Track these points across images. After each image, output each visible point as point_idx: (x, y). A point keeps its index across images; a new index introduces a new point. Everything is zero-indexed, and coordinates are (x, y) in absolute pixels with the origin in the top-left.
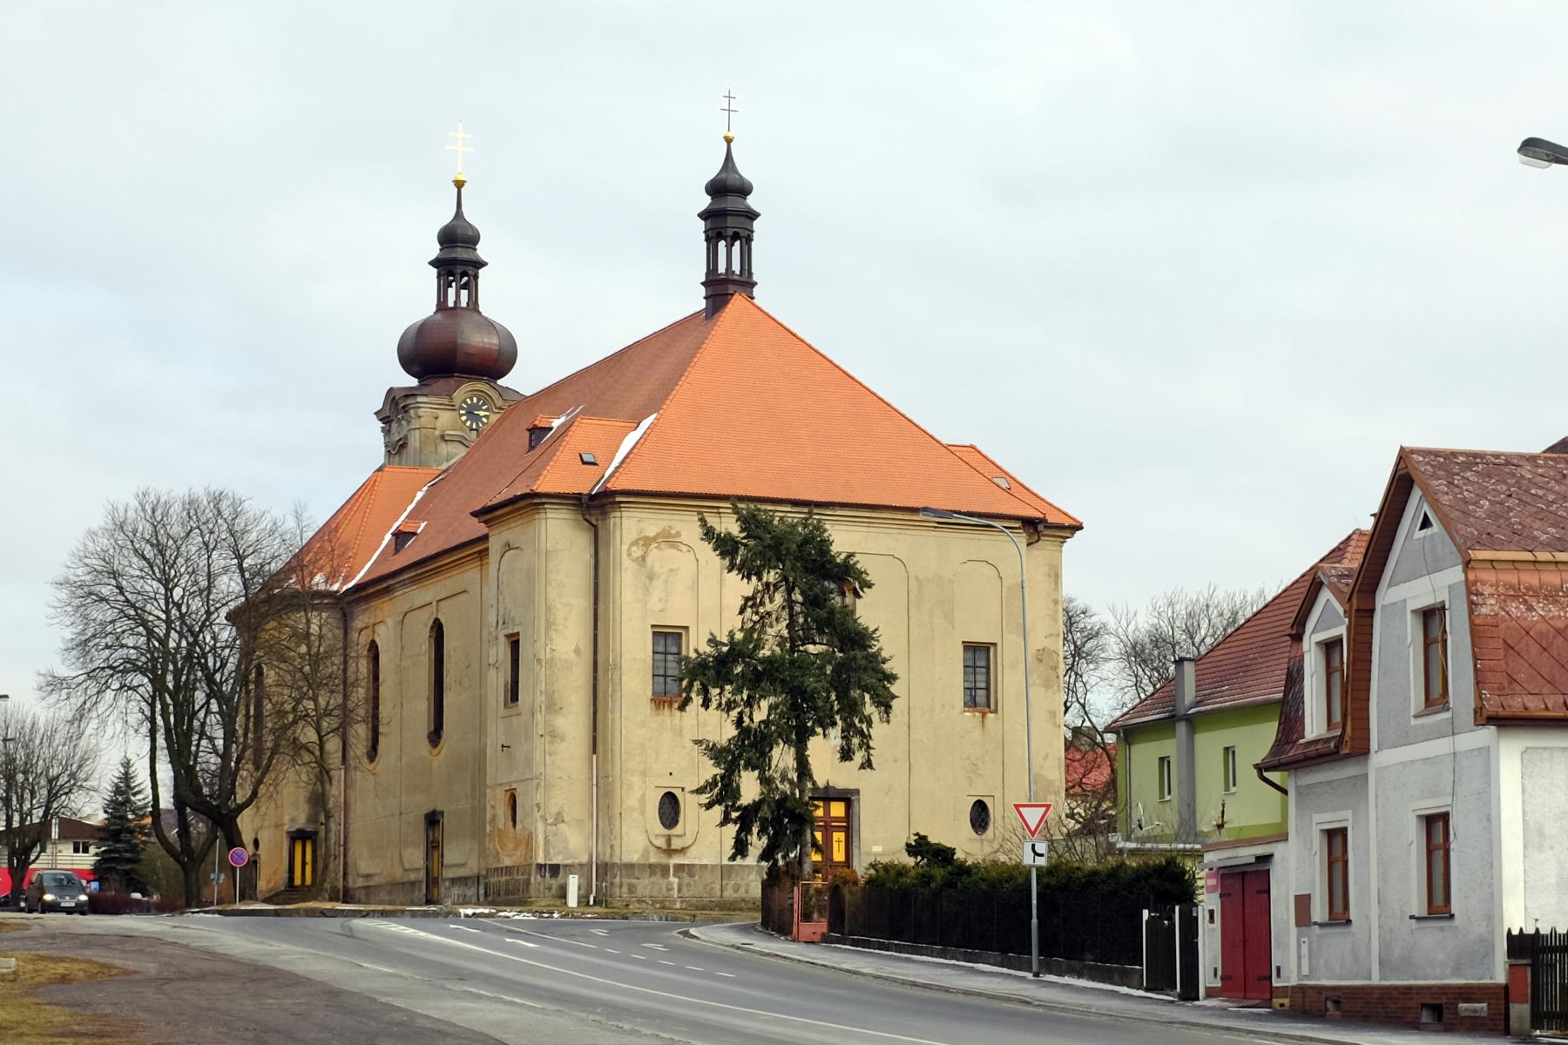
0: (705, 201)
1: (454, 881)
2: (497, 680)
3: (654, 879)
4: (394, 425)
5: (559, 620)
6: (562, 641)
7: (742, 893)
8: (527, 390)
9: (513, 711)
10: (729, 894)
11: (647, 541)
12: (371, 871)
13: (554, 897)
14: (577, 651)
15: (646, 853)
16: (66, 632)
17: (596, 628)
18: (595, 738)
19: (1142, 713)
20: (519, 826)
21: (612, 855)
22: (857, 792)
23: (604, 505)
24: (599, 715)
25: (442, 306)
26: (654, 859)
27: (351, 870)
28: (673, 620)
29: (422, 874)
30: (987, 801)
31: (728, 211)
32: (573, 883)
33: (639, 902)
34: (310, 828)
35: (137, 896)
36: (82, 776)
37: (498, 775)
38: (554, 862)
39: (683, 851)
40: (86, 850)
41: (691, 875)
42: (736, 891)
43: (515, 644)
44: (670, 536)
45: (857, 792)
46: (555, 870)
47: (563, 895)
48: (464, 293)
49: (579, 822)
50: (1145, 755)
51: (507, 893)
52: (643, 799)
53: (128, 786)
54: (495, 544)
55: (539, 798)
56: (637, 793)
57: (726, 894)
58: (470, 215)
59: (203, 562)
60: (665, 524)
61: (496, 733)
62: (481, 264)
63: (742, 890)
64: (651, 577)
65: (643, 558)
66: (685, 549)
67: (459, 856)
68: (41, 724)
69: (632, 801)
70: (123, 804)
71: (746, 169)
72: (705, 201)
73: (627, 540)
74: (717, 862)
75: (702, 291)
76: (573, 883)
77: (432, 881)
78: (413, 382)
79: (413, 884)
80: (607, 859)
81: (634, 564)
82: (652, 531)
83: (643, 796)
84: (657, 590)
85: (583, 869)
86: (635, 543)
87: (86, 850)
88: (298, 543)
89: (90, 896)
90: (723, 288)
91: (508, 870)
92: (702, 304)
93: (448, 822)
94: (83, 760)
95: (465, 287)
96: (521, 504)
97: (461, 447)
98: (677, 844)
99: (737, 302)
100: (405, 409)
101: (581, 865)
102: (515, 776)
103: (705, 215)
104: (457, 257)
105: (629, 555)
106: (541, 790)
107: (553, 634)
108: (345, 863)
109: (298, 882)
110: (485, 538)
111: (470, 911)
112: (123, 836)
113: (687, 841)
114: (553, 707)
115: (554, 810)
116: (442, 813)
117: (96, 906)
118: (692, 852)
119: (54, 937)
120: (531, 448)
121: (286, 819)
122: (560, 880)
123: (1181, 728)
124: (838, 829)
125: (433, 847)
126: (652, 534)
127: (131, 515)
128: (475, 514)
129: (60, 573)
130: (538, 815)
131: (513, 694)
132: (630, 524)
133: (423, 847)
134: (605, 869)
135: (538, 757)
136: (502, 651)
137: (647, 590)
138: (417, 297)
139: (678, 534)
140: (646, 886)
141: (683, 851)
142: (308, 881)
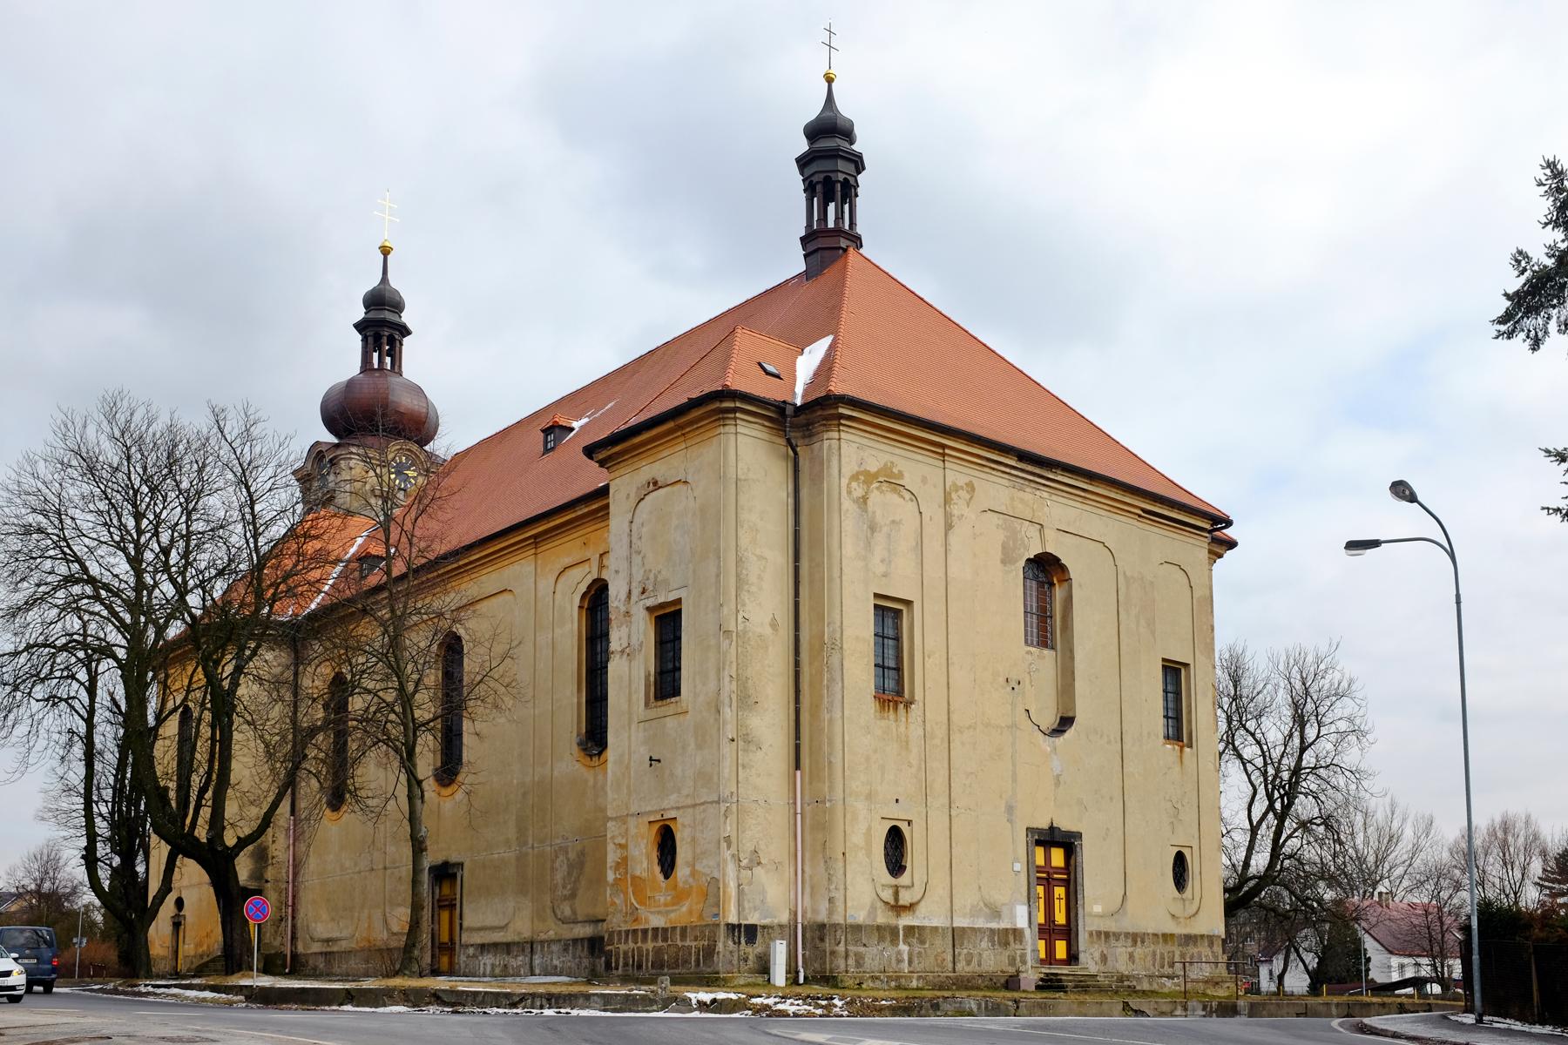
1: (483, 948)
5: (753, 579)
6: (749, 612)
11: (868, 478)
12: (335, 935)
13: (751, 971)
14: (774, 625)
15: (873, 908)
17: (797, 594)
20: (682, 871)
21: (831, 912)
22: (1079, 835)
26: (883, 918)
31: (830, 159)
39: (911, 907)
41: (922, 942)
44: (892, 475)
45: (1079, 835)
46: (751, 932)
47: (764, 968)
49: (777, 865)
54: (619, 503)
55: (729, 829)
56: (863, 827)
57: (959, 967)
58: (394, 282)
60: (887, 458)
62: (405, 331)
63: (975, 960)
64: (873, 528)
65: (865, 499)
66: (908, 496)
69: (857, 838)
71: (846, 108)
72: (803, 146)
73: (849, 468)
74: (948, 924)
80: (822, 917)
81: (855, 507)
82: (873, 466)
83: (869, 829)
84: (880, 538)
85: (788, 931)
86: (855, 477)
89: (1338, 902)
90: (828, 245)
98: (905, 898)
100: (333, 462)
101: (781, 926)
102: (672, 800)
104: (382, 326)
105: (849, 493)
106: (732, 818)
107: (745, 596)
108: (294, 926)
110: (603, 492)
111: (706, 997)
114: (746, 701)
115: (749, 847)
118: (922, 909)
120: (547, 451)
122: (758, 948)
126: (873, 469)
128: (590, 451)
130: (728, 854)
131: (666, 683)
132: (851, 452)
134: (819, 932)
135: (727, 769)
137: (868, 545)
139: (901, 474)
140: (875, 956)
141: (911, 907)
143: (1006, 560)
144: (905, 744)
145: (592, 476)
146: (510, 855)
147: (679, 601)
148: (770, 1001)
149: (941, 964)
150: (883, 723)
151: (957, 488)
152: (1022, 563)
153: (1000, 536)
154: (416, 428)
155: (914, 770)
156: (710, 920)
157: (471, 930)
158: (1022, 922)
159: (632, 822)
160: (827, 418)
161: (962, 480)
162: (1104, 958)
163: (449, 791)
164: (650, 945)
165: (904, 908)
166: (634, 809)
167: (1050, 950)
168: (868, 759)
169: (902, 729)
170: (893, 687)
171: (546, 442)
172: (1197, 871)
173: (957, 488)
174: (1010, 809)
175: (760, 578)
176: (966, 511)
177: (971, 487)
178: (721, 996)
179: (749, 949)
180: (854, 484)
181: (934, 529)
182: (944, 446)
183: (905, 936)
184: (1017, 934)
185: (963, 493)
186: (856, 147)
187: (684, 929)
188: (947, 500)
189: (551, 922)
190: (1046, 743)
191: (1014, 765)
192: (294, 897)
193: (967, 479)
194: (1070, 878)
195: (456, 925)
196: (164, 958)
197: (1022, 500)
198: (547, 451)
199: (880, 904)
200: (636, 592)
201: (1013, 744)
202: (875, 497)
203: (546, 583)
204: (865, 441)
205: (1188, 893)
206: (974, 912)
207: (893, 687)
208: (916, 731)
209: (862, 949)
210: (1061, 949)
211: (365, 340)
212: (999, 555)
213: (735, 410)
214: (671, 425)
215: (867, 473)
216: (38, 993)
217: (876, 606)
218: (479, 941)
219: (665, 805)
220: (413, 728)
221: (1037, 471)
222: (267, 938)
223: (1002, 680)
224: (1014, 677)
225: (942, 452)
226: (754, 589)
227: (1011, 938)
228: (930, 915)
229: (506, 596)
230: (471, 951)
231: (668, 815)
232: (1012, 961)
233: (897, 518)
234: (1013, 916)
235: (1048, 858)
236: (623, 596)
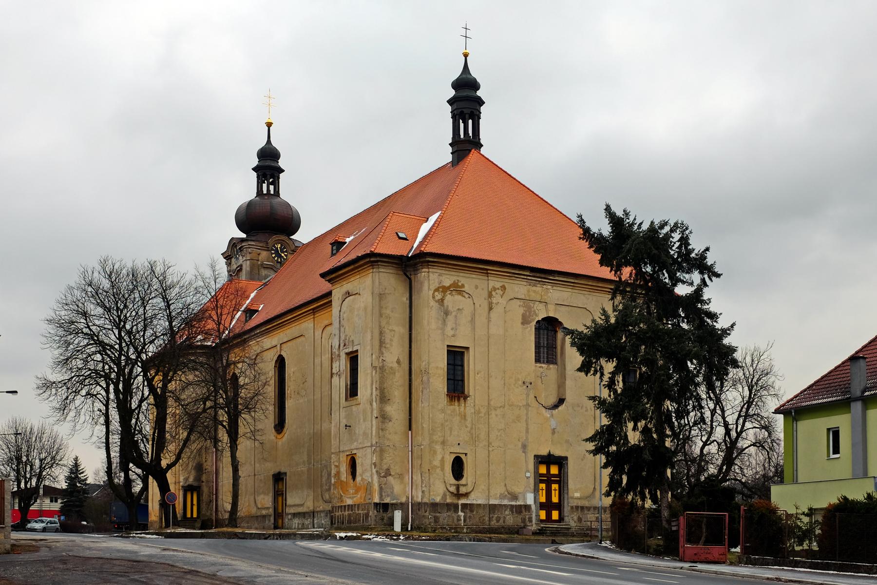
0: (452, 93)
1: (295, 515)
4: (233, 260)
5: (387, 341)
8: (305, 241)
9: (354, 402)
10: (494, 523)
11: (444, 289)
13: (385, 525)
14: (398, 362)
15: (445, 495)
16: (57, 353)
18: (410, 420)
19: (806, 399)
20: (358, 479)
22: (566, 458)
23: (416, 264)
24: (413, 405)
25: (259, 192)
27: (220, 509)
28: (460, 343)
29: (271, 511)
31: (466, 100)
32: (398, 515)
33: (442, 528)
34: (195, 484)
35: (85, 523)
36: (58, 458)
39: (466, 495)
40: (56, 501)
41: (472, 511)
42: (498, 521)
45: (566, 458)
47: (392, 524)
50: (813, 430)
51: (350, 522)
52: (442, 461)
53: (77, 470)
54: (338, 293)
57: (492, 523)
58: (275, 143)
59: (141, 311)
60: (455, 278)
64: (447, 313)
65: (442, 300)
66: (467, 296)
68: (35, 430)
70: (74, 478)
71: (475, 73)
72: (452, 93)
73: (433, 288)
75: (450, 149)
76: (398, 515)
77: (278, 515)
78: (244, 236)
79: (264, 517)
82: (447, 281)
83: (443, 458)
84: (451, 318)
86: (437, 290)
87: (56, 501)
88: (214, 287)
90: (465, 145)
92: (449, 158)
93: (289, 480)
94: (59, 449)
95: (272, 183)
97: (272, 272)
98: (463, 490)
99: (473, 156)
101: (401, 504)
102: (355, 445)
103: (451, 102)
104: (268, 166)
105: (434, 297)
107: (384, 350)
109: (189, 515)
111: (343, 535)
112: (75, 494)
115: (385, 467)
117: (65, 528)
118: (472, 496)
119: (64, 561)
120: (333, 255)
121: (182, 479)
123: (857, 407)
124: (555, 482)
125: (279, 494)
128: (323, 275)
129: (51, 314)
132: (431, 279)
136: (342, 364)
137: (444, 322)
138: (245, 189)
139: (463, 286)
141: (466, 495)
142: (195, 515)
143: (525, 321)
144: (464, 417)
145: (324, 286)
146: (305, 469)
147: (357, 351)
148: (371, 537)
149: (483, 524)
150: (452, 407)
151: (495, 289)
152: (534, 323)
153: (521, 311)
154: (288, 223)
155: (468, 429)
156: (368, 501)
157: (290, 506)
158: (530, 500)
160: (422, 262)
161: (498, 285)
162: (580, 520)
163: (281, 436)
164: (347, 513)
167: (549, 515)
169: (462, 409)
170: (456, 388)
171: (332, 250)
173: (495, 289)
174: (524, 447)
175: (391, 340)
176: (501, 300)
177: (503, 288)
178: (350, 534)
179: (385, 515)
180: (436, 293)
181: (483, 310)
182: (487, 270)
184: (527, 507)
185: (500, 292)
186: (479, 93)
187: (358, 505)
188: (490, 295)
189: (321, 501)
190: (547, 414)
191: (527, 424)
192: (217, 490)
193: (501, 284)
194: (561, 480)
196: (156, 522)
197: (534, 292)
198: (333, 255)
200: (342, 345)
201: (527, 414)
202: (449, 298)
203: (318, 333)
204: (443, 272)
206: (502, 497)
207: (456, 388)
209: (438, 515)
210: (555, 515)
212: (520, 321)
213: (377, 261)
214: (352, 267)
215: (444, 287)
217: (448, 351)
219: (353, 447)
220: (216, 422)
221: (543, 276)
222: (203, 511)
223: (520, 383)
224: (528, 380)
225: (486, 273)
226: (388, 346)
227: (523, 510)
228: (476, 499)
229: (302, 338)
230: (290, 517)
231: (354, 452)
232: (524, 521)
233: (461, 307)
234: (525, 499)
235: (548, 470)
236: (337, 347)
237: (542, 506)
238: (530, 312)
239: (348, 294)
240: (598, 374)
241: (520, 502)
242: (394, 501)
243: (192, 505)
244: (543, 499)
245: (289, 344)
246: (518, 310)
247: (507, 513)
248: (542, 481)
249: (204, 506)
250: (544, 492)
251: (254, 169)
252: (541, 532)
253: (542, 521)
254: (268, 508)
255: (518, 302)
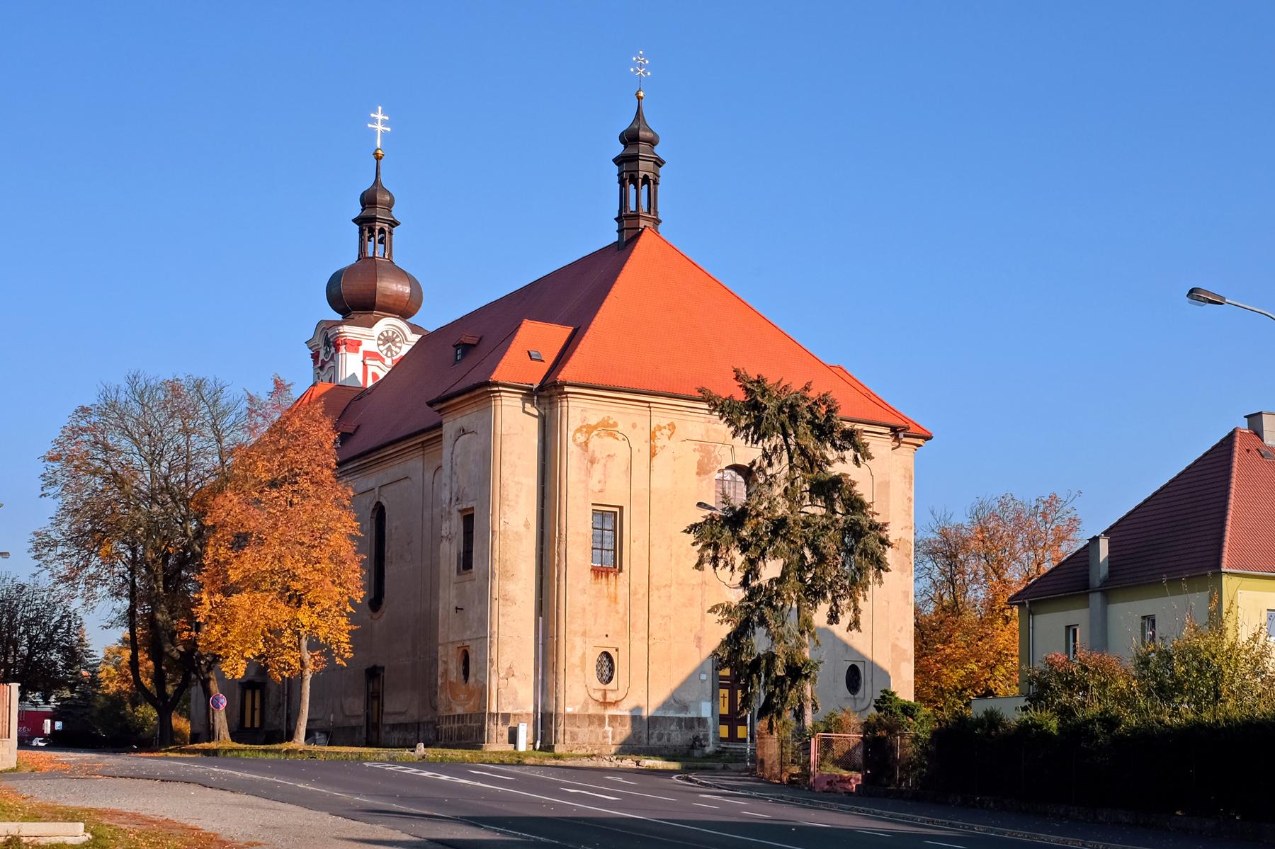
0: (619, 149)
1: (394, 727)
2: (450, 551)
3: (592, 728)
5: (511, 497)
7: (664, 741)
9: (468, 577)
10: (654, 741)
11: (589, 429)
14: (527, 525)
15: (586, 705)
20: (471, 680)
26: (594, 710)
29: (362, 721)
30: (858, 665)
34: (258, 680)
37: (449, 633)
38: (506, 711)
39: (615, 703)
42: (660, 740)
43: (468, 519)
44: (609, 425)
48: (380, 247)
51: (460, 737)
54: (449, 428)
56: (579, 653)
57: (652, 742)
58: (385, 182)
60: (605, 415)
61: (448, 597)
63: (665, 737)
64: (592, 462)
65: (586, 443)
67: (398, 705)
71: (654, 122)
78: (339, 317)
79: (353, 728)
82: (593, 421)
83: (584, 654)
84: (598, 468)
86: (579, 430)
91: (461, 718)
96: (478, 392)
98: (611, 697)
102: (468, 634)
103: (619, 161)
104: (373, 217)
105: (574, 440)
107: (505, 508)
109: (248, 725)
113: (620, 695)
116: (383, 668)
123: (1096, 599)
125: (374, 698)
126: (593, 422)
127: (123, 397)
131: (466, 562)
133: (363, 697)
137: (588, 473)
139: (615, 424)
141: (615, 703)
142: (257, 725)
143: (702, 470)
147: (472, 509)
153: (697, 456)
155: (620, 616)
158: (706, 711)
159: (450, 646)
164: (456, 725)
165: (610, 704)
166: (451, 639)
167: (733, 732)
168: (584, 610)
169: (612, 588)
172: (868, 679)
173: (660, 428)
174: (699, 639)
175: (517, 496)
177: (672, 427)
180: (578, 435)
183: (610, 721)
184: (701, 721)
188: (652, 436)
195: (380, 711)
199: (590, 701)
202: (595, 442)
205: (860, 694)
207: (609, 565)
208: (623, 591)
209: (576, 729)
211: (361, 232)
212: (695, 470)
216: (38, 748)
218: (391, 722)
227: (696, 724)
231: (467, 643)
234: (699, 710)
237: (723, 719)
238: (709, 459)
239: (463, 431)
240: (729, 568)
241: (692, 714)
242: (518, 711)
243: (253, 709)
244: (724, 710)
245: (391, 488)
246: (692, 458)
247: (673, 728)
248: (722, 686)
249: (270, 712)
250: (727, 700)
251: (354, 221)
252: (717, 755)
253: (722, 740)
254: (358, 716)
255: (693, 445)
